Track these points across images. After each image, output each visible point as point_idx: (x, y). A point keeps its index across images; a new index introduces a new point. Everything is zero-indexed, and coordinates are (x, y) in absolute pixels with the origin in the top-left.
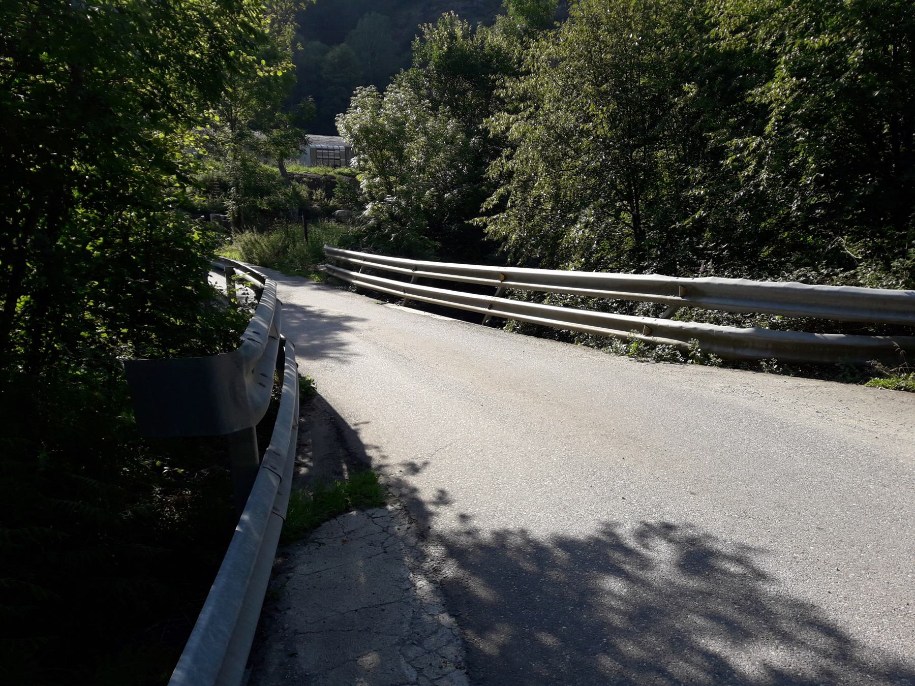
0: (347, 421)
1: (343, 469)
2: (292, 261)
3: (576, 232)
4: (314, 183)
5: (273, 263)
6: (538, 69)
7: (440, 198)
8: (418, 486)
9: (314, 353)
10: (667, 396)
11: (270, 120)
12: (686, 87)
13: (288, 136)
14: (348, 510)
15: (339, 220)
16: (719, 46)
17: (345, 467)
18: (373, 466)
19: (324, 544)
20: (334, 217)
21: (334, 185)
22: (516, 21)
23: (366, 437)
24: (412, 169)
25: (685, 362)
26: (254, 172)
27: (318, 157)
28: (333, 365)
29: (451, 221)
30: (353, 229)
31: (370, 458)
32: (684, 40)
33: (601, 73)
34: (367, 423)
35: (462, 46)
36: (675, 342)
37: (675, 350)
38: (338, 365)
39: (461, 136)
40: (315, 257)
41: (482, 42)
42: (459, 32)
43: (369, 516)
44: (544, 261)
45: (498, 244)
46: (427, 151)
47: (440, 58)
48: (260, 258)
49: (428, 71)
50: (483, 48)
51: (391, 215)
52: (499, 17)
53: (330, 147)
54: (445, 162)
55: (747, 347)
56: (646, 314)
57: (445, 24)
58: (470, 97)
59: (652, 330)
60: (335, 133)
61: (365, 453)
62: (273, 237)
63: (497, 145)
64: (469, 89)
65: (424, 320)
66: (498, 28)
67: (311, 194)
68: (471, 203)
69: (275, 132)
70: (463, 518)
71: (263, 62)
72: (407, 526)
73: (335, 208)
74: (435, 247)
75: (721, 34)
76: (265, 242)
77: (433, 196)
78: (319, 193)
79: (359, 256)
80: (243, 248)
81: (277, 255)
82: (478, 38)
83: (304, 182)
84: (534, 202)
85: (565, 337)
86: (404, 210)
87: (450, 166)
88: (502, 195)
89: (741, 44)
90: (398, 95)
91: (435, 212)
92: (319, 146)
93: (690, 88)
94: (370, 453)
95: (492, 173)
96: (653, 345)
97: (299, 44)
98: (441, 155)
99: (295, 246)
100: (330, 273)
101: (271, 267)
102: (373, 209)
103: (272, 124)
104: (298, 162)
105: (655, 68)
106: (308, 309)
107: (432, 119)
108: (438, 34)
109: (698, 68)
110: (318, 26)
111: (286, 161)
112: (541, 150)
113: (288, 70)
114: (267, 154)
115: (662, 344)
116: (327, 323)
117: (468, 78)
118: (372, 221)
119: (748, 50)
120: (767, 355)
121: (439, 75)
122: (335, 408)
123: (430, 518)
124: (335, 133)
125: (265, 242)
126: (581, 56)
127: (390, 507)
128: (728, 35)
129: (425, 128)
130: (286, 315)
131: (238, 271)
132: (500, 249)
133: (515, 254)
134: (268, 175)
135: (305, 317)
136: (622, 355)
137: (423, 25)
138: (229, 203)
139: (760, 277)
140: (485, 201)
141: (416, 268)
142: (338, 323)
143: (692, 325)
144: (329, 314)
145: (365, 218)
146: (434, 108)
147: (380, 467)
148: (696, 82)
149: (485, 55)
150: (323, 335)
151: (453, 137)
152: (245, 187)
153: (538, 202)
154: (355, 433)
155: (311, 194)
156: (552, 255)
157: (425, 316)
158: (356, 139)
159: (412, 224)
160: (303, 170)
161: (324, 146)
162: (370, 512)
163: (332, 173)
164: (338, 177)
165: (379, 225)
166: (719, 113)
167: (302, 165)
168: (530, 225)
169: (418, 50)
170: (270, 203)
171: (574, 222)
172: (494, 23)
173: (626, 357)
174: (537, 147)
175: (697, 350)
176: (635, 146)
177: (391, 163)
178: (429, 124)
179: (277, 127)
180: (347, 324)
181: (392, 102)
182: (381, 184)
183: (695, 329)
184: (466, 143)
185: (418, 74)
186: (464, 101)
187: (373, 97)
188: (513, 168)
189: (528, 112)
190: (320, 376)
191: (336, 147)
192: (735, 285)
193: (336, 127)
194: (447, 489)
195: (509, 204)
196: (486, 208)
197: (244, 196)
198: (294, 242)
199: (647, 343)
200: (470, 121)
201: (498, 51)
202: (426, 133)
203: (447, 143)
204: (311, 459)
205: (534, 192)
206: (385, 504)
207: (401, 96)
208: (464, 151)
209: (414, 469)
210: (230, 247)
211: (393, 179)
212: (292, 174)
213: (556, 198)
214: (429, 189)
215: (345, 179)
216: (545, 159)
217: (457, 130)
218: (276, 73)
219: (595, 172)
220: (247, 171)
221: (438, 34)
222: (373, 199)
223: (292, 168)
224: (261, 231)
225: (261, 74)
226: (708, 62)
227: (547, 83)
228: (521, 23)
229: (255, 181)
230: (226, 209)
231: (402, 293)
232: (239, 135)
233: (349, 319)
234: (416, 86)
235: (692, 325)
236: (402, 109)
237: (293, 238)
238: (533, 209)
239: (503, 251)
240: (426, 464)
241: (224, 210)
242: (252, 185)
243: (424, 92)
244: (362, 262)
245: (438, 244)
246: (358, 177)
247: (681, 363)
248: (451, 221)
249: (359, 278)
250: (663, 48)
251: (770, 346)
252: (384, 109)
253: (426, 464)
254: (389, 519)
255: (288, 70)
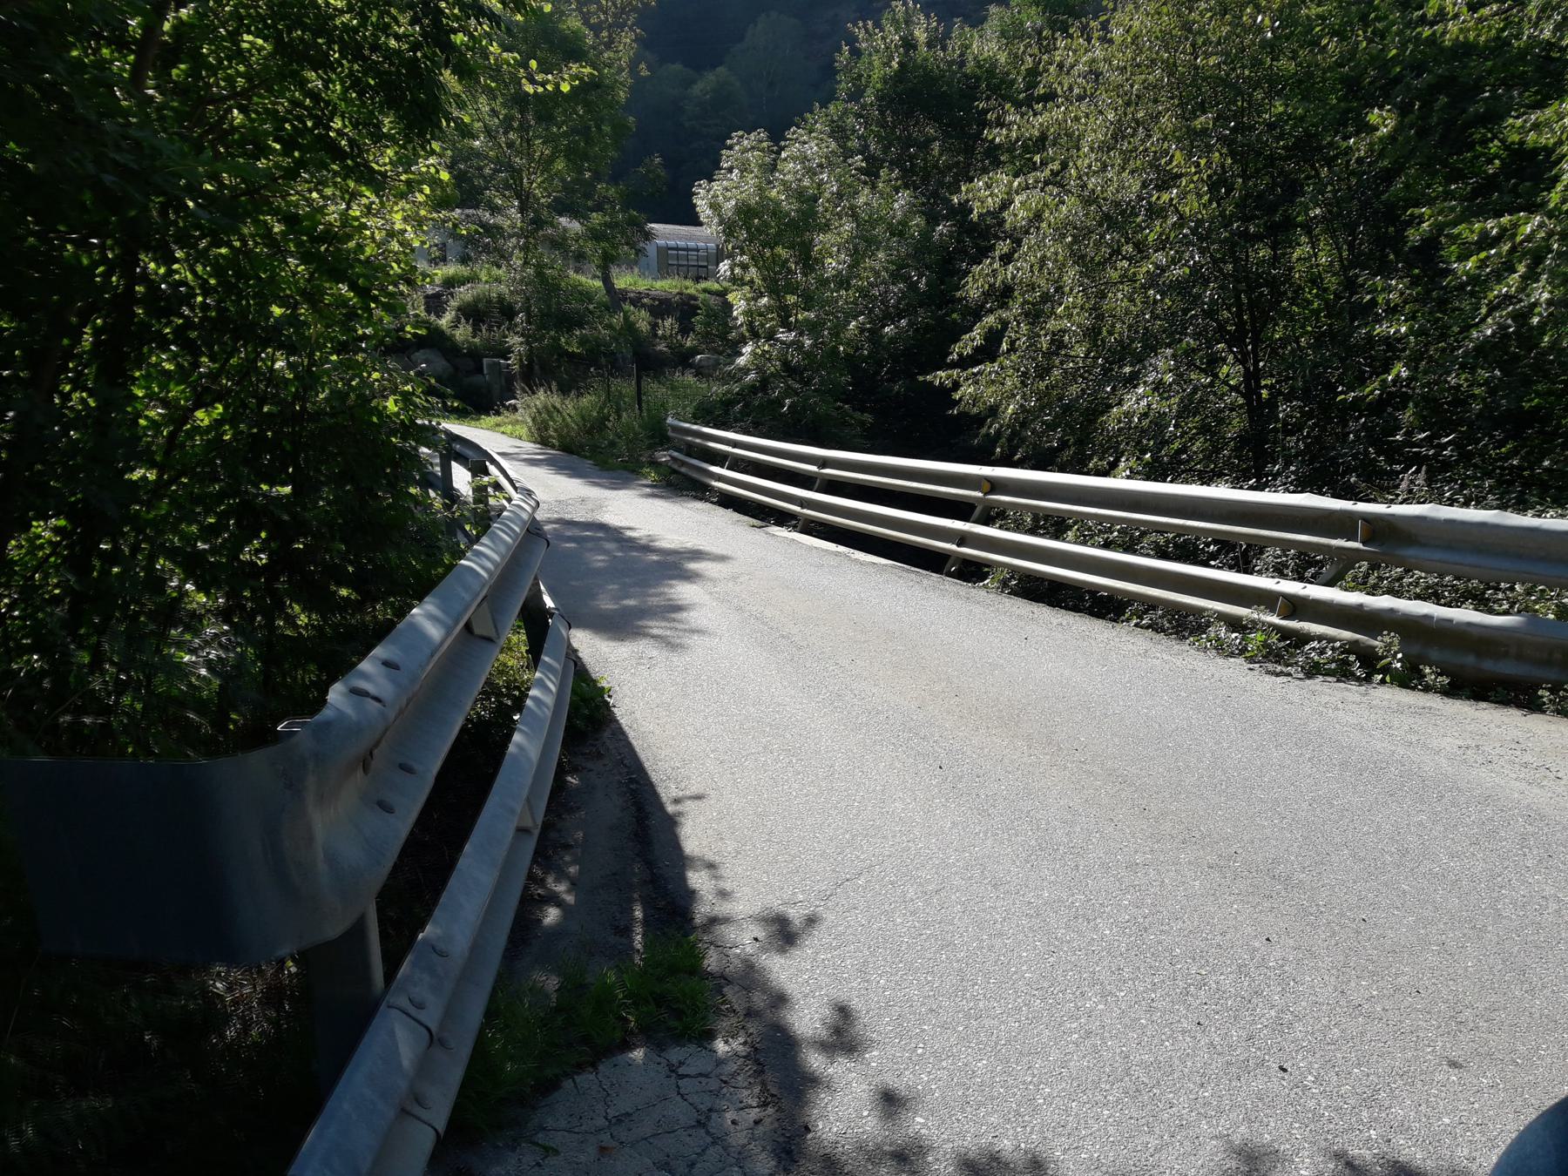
0: (661, 790)
1: (633, 919)
2: (613, 444)
3: (1137, 401)
4: (661, 308)
5: (582, 447)
6: (1071, 89)
7: (875, 334)
8: (791, 988)
9: (620, 626)
10: (1344, 765)
11: (588, 196)
12: (1374, 116)
13: (617, 224)
14: (627, 1046)
15: (700, 372)
16: (1444, 33)
17: (638, 914)
18: (698, 920)
19: (556, 1152)
20: (691, 366)
21: (694, 310)
22: (1024, 16)
23: (694, 837)
24: (827, 281)
25: (1368, 679)
26: (557, 288)
27: (670, 261)
28: (655, 653)
29: (893, 376)
30: (718, 390)
31: (691, 894)
32: (1366, 25)
33: (1192, 93)
34: (698, 797)
35: (926, 60)
36: (1347, 635)
37: (1349, 652)
38: (665, 653)
39: (918, 220)
40: (652, 437)
41: (962, 55)
42: (921, 35)
43: (672, 1069)
44: (1067, 454)
45: (979, 420)
46: (856, 250)
47: (885, 82)
48: (560, 436)
49: (863, 107)
50: (962, 64)
51: (786, 364)
52: (993, 9)
53: (691, 244)
54: (886, 269)
55: (1506, 655)
56: (1279, 571)
57: (895, 22)
58: (936, 152)
59: (1296, 607)
60: (695, 221)
61: (684, 879)
62: (586, 401)
63: (980, 236)
64: (935, 139)
65: (833, 561)
66: (992, 26)
67: (654, 326)
68: (931, 347)
69: (596, 218)
70: (891, 1102)
71: (533, 64)
72: (754, 1114)
73: (694, 351)
74: (862, 423)
75: (1449, 9)
76: (572, 408)
77: (862, 331)
78: (668, 324)
79: (726, 438)
80: (534, 419)
81: (589, 432)
82: (954, 45)
83: (643, 305)
84: (1052, 342)
85: (1107, 607)
86: (808, 355)
87: (896, 276)
88: (991, 328)
89: (1490, 28)
90: (808, 145)
91: (865, 359)
92: (672, 243)
93: (1383, 120)
94: (697, 879)
95: (973, 289)
96: (1302, 639)
97: (643, 66)
98: (881, 255)
99: (620, 417)
100: (675, 467)
101: (578, 454)
102: (753, 353)
103: (590, 203)
104: (636, 270)
105: (1304, 86)
106: (629, 533)
107: (866, 191)
108: (883, 38)
109: (1397, 80)
110: (678, 38)
111: (614, 271)
112: (1072, 243)
113: (581, 80)
114: (580, 257)
115: (1320, 638)
116: (657, 562)
117: (936, 119)
118: (752, 376)
119: (1500, 44)
120: (1553, 674)
121: (882, 113)
122: (642, 756)
123: (811, 1095)
124: (695, 221)
125: (572, 408)
126: (1153, 61)
127: (721, 1046)
128: (1465, 9)
129: (852, 208)
130: (590, 545)
131: (492, 468)
132: (984, 431)
133: (1010, 440)
134: (581, 293)
135: (621, 549)
136: (1232, 655)
137: (855, 25)
138: (514, 340)
139: (1521, 506)
140: (959, 340)
141: (824, 463)
142: (676, 565)
143: (1384, 602)
144: (664, 544)
145: (740, 369)
146: (871, 172)
147: (714, 921)
148: (1394, 105)
149: (965, 75)
150: (638, 588)
151: (904, 223)
152: (543, 315)
153: (1058, 343)
154: (671, 823)
155: (654, 326)
156: (1081, 443)
157: (837, 554)
158: (729, 229)
159: (822, 383)
160: (643, 285)
161: (681, 244)
162: (675, 1054)
163: (692, 291)
164: (701, 296)
165: (764, 383)
166: (221, 555)
167: (642, 275)
168: (1042, 385)
169: (847, 69)
170: (583, 342)
171: (1132, 381)
172: (983, 20)
173: (1241, 660)
174: (1064, 236)
175: (1394, 656)
176: (1258, 238)
177: (790, 271)
178: (861, 200)
179: (598, 208)
180: (693, 566)
181: (794, 159)
182: (769, 309)
183: (1392, 610)
184: (926, 234)
185: (846, 112)
186: (924, 159)
187: (762, 150)
188: (1014, 277)
189: (1047, 172)
190: (627, 676)
191: (701, 244)
192: (1483, 525)
193: (695, 206)
194: (856, 1004)
195: (1004, 346)
196: (960, 355)
197: (539, 329)
198: (618, 413)
199: (1285, 634)
200: (935, 194)
201: (989, 68)
202: (855, 216)
203: (893, 235)
204: (574, 885)
205: (1052, 324)
206: (710, 1036)
207: (812, 148)
208: (923, 247)
209: (784, 933)
210: (513, 417)
211: (791, 299)
212: (624, 292)
213: (1092, 334)
214: (855, 318)
215: (713, 301)
216: (1080, 259)
217: (911, 211)
218: (557, 86)
219: (1180, 287)
220: (545, 286)
221: (883, 38)
222: (755, 335)
223: (624, 280)
224: (564, 390)
225: (529, 89)
226: (1418, 68)
227: (1087, 116)
228: (1032, 19)
229: (558, 303)
230: (509, 350)
231: (798, 509)
232: (533, 222)
233: (697, 555)
234: (839, 132)
235: (1384, 602)
236: (811, 172)
237: (618, 404)
238: (1048, 355)
239: (988, 435)
240: (811, 921)
241: (505, 353)
242: (554, 311)
243: (854, 143)
244: (729, 449)
245: (868, 418)
246: (730, 297)
247: (1358, 679)
248: (893, 376)
249: (724, 477)
250: (1324, 42)
251: (1557, 656)
252: (781, 172)
253: (811, 921)
254: (714, 1084)
255: (581, 80)
